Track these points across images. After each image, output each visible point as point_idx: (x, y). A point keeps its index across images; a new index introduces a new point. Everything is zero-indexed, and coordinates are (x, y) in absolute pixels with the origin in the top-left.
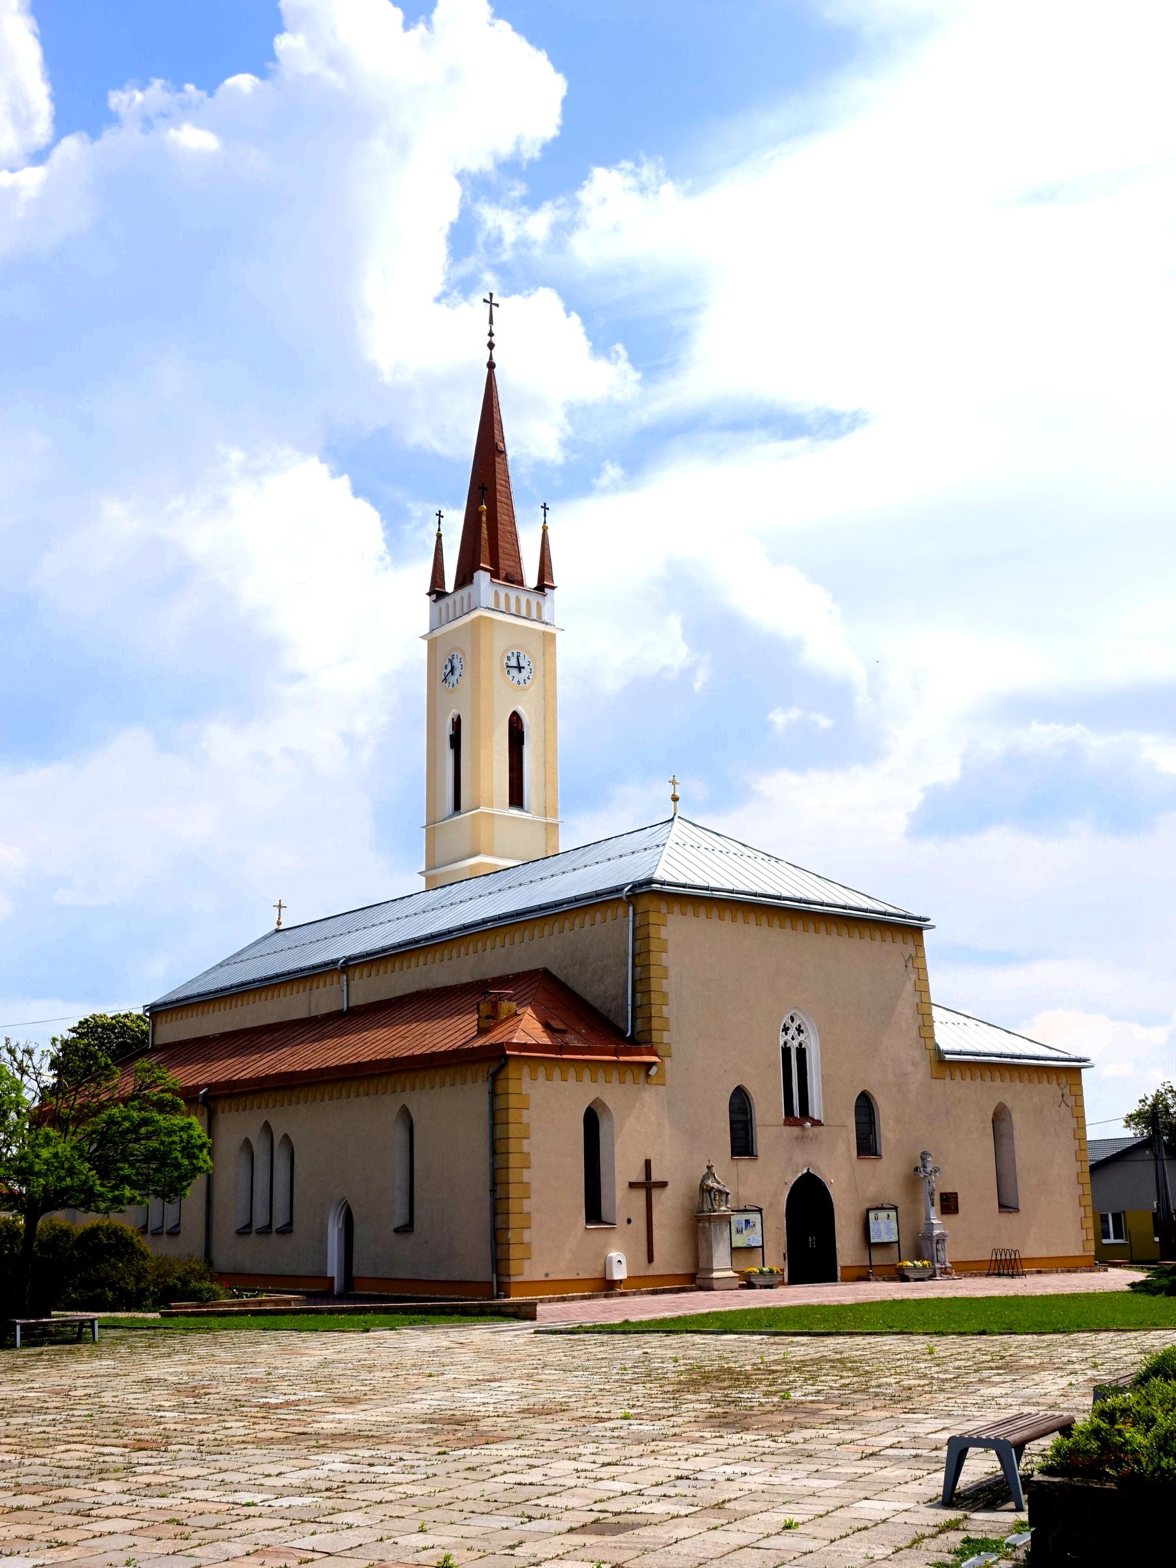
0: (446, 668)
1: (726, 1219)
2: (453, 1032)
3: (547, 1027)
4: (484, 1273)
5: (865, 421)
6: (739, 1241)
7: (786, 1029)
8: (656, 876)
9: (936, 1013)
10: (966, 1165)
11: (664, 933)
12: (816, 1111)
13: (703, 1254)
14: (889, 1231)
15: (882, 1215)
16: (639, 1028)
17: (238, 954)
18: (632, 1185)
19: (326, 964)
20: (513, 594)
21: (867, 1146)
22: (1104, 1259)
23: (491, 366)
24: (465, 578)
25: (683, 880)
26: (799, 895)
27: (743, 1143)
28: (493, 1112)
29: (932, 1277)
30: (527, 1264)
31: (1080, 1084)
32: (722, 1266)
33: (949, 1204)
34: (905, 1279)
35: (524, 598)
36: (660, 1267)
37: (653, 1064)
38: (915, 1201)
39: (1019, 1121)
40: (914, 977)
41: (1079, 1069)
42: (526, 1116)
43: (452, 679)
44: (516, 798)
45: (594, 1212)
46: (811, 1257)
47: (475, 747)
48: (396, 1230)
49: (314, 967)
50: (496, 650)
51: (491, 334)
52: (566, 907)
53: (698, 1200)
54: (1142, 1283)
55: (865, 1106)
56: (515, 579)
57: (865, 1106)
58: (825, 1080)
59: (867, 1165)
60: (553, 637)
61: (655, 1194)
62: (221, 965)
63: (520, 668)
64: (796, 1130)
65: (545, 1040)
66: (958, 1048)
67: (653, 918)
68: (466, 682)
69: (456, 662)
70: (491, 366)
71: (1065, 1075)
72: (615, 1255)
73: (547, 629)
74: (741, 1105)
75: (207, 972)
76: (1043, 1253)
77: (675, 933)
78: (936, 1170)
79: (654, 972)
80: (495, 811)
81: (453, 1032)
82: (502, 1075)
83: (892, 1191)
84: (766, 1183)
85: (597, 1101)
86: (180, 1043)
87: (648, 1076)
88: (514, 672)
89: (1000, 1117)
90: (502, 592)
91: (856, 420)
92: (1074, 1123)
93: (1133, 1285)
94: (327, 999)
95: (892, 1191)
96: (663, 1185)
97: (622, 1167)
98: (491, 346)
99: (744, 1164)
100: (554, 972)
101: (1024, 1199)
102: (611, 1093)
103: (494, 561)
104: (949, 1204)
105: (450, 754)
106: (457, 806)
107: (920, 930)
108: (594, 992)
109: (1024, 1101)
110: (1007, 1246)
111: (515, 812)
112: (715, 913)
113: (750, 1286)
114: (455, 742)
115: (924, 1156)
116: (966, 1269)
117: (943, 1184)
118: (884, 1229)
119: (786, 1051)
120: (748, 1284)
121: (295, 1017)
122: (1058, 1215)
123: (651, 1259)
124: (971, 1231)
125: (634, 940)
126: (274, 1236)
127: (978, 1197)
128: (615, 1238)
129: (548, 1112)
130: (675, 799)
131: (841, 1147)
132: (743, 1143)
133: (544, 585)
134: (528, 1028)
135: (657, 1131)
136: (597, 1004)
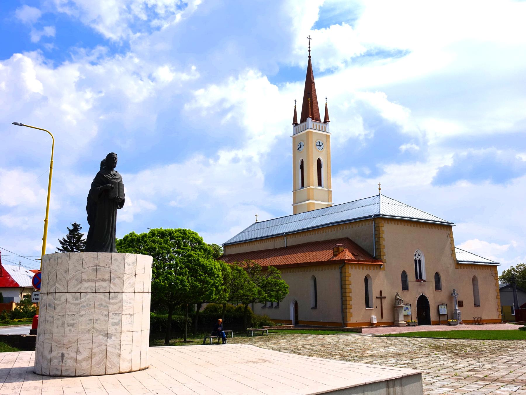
0: (299, 146)
1: (402, 307)
2: (326, 255)
3: (353, 254)
4: (339, 320)
5: (410, 52)
6: (405, 313)
7: (415, 255)
8: (381, 213)
9: (456, 250)
10: (465, 293)
11: (383, 229)
12: (424, 277)
13: (396, 317)
14: (445, 311)
15: (443, 307)
16: (377, 255)
17: (246, 229)
18: (377, 298)
19: (279, 234)
20: (318, 124)
21: (438, 287)
22: (504, 320)
23: (310, 57)
24: (303, 120)
25: (388, 214)
26: (418, 218)
27: (405, 287)
28: (341, 278)
29: (457, 324)
30: (351, 318)
31: (497, 270)
32: (402, 321)
33: (461, 304)
34: (450, 325)
35: (321, 125)
36: (384, 320)
37: (381, 265)
38: (451, 303)
39: (480, 281)
40: (450, 240)
41: (496, 266)
42: (350, 279)
43: (300, 149)
44: (320, 184)
45: (367, 305)
46: (424, 318)
47: (305, 168)
48: (312, 308)
49: (276, 235)
50: (314, 141)
51: (309, 48)
52: (353, 221)
53: (394, 302)
54: (522, 328)
55: (437, 276)
56: (318, 119)
57: (437, 276)
58: (426, 269)
59: (438, 293)
60: (329, 136)
61: (383, 300)
62: (242, 232)
63: (320, 146)
64: (419, 283)
65: (354, 258)
66: (462, 260)
67: (380, 225)
68: (305, 150)
69: (301, 144)
70: (310, 57)
71: (493, 267)
72: (373, 316)
73: (328, 134)
74: (404, 275)
75: (238, 235)
76: (487, 318)
77: (386, 229)
78: (457, 294)
79: (381, 239)
80: (314, 187)
81: (326, 255)
82: (344, 268)
83: (445, 301)
84: (411, 298)
85: (368, 275)
86: (234, 255)
87: (380, 268)
88: (318, 147)
89: (474, 279)
90: (315, 124)
91: (407, 53)
92: (495, 281)
93: (520, 328)
94: (279, 244)
95: (445, 301)
96: (385, 297)
97: (374, 293)
98: (309, 51)
99: (406, 292)
100: (350, 238)
101: (481, 302)
102: (371, 272)
103: (312, 115)
104: (461, 304)
105: (300, 171)
106: (303, 186)
107: (451, 226)
108: (363, 244)
109: (480, 274)
110: (477, 316)
111: (319, 188)
112: (396, 223)
113: (409, 325)
114: (302, 167)
115: (454, 290)
116: (466, 322)
117: (459, 298)
118: (443, 310)
119: (416, 261)
120: (408, 325)
121: (270, 248)
122: (491, 307)
123: (382, 318)
124: (467, 311)
125: (375, 231)
126: (273, 309)
127: (469, 302)
128: (373, 312)
129: (356, 277)
130: (380, 189)
131: (431, 287)
132: (405, 287)
133: (326, 121)
134: (348, 255)
135: (384, 283)
136: (364, 248)
